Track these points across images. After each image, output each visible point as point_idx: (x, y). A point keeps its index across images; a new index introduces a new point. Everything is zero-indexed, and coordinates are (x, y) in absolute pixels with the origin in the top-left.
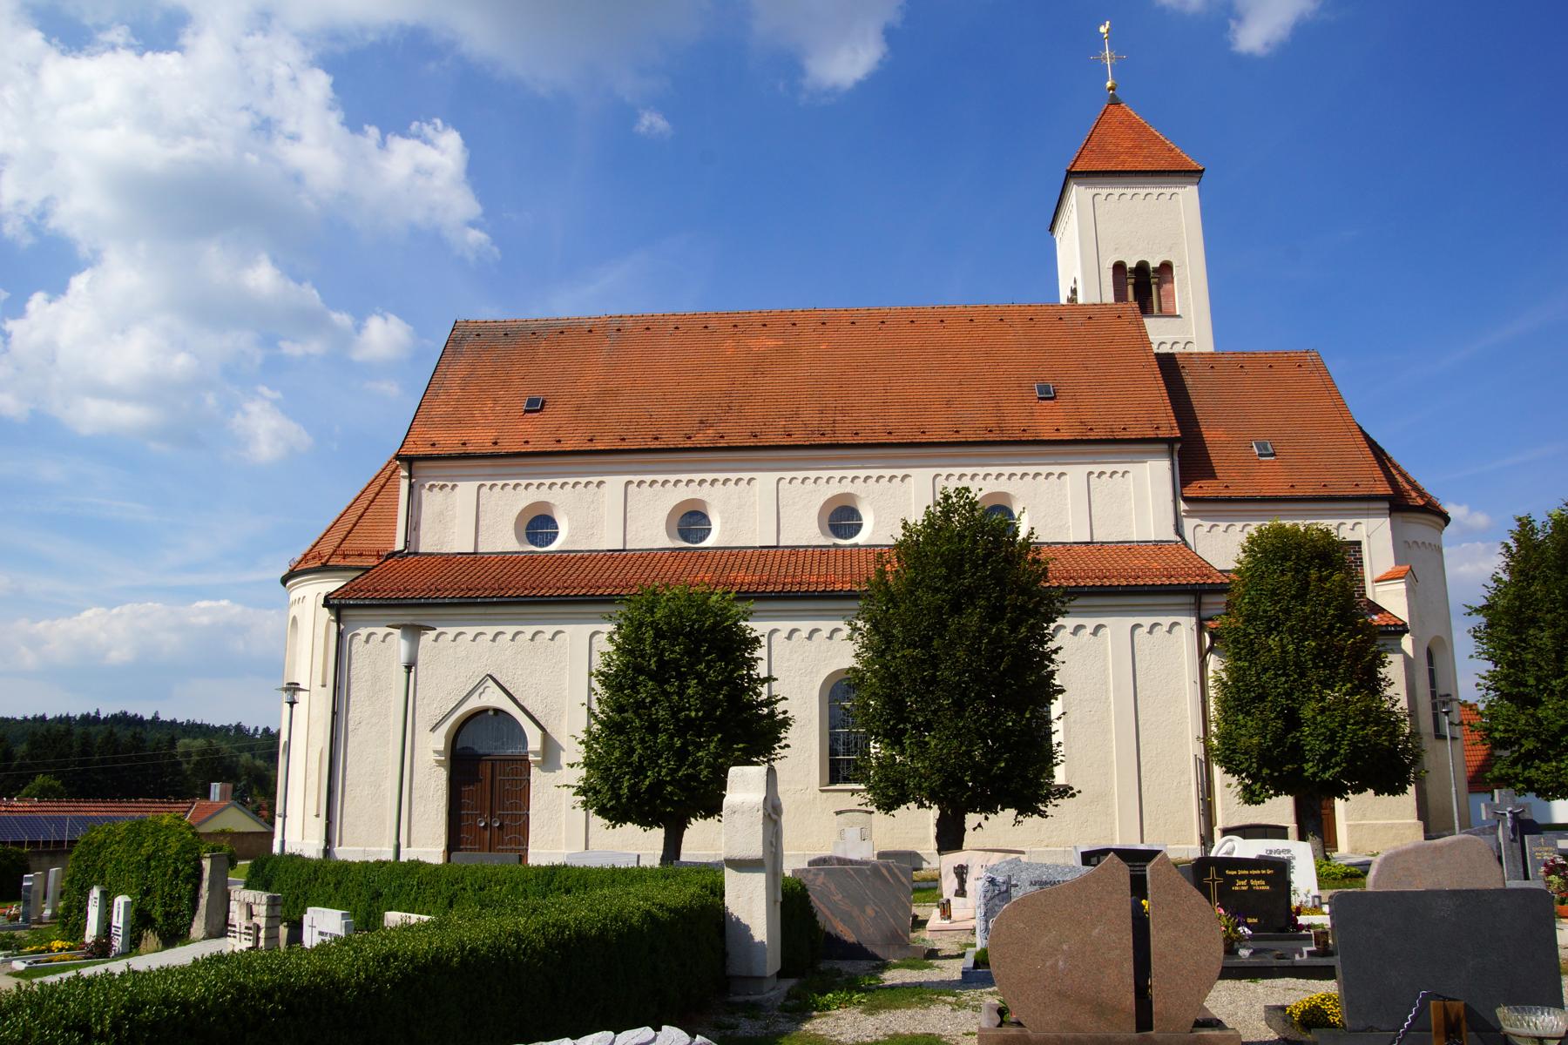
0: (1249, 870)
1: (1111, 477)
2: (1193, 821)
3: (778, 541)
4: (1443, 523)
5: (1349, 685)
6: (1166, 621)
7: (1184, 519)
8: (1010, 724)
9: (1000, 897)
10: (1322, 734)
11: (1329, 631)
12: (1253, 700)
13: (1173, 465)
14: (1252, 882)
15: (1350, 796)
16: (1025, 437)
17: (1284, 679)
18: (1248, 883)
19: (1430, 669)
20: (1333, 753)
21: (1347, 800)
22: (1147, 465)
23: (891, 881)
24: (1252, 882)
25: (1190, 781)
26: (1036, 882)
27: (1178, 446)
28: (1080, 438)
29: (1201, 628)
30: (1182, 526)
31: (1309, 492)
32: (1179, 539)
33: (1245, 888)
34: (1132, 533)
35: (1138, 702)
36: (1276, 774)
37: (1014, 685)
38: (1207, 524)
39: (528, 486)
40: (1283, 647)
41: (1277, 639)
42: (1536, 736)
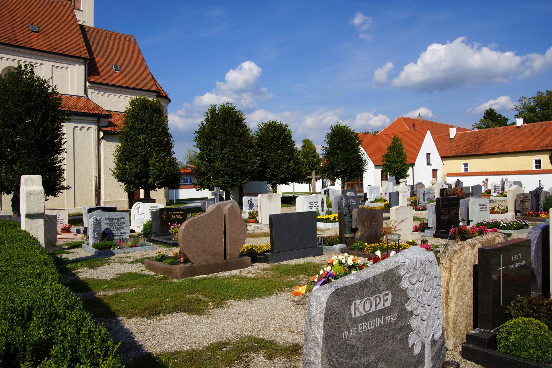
0: (176, 212)
1: (61, 68)
2: (93, 198)
3: (294, 190)
4: (169, 102)
5: (165, 154)
6: (87, 126)
7: (88, 89)
8: (50, 161)
9: (99, 224)
10: (157, 169)
11: (159, 135)
12: (132, 157)
13: (85, 68)
14: (177, 216)
15: (158, 190)
16: (27, 46)
17: (144, 150)
18: (176, 217)
19: (540, 163)
20: (160, 175)
21: (156, 191)
22: (76, 66)
23: (49, 221)
24: (177, 216)
25: (92, 184)
26: (107, 219)
27: (88, 61)
28: (50, 51)
29: (99, 130)
30: (87, 92)
31: (132, 86)
32: (86, 96)
33: (175, 218)
34: (68, 91)
35: (75, 155)
36: (140, 182)
37: (51, 146)
38: (96, 92)
39: (8, 59)
40: (144, 139)
41: (142, 136)
42: (213, 172)
